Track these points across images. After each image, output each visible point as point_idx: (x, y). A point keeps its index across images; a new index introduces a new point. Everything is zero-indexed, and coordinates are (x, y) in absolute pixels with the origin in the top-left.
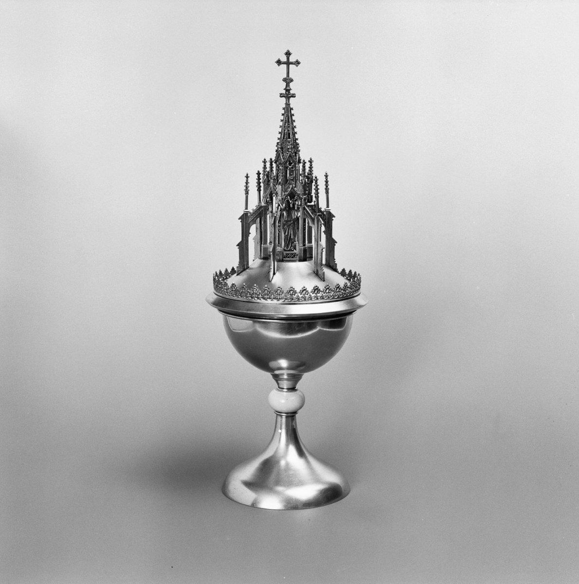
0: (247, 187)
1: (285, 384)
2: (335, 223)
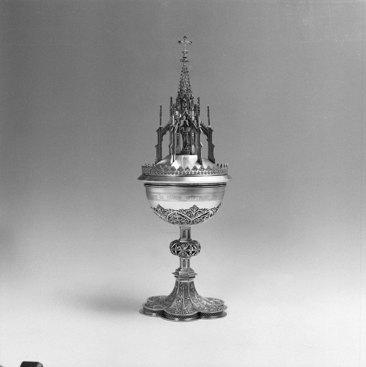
0: (161, 113)
1: (176, 254)
2: (214, 135)
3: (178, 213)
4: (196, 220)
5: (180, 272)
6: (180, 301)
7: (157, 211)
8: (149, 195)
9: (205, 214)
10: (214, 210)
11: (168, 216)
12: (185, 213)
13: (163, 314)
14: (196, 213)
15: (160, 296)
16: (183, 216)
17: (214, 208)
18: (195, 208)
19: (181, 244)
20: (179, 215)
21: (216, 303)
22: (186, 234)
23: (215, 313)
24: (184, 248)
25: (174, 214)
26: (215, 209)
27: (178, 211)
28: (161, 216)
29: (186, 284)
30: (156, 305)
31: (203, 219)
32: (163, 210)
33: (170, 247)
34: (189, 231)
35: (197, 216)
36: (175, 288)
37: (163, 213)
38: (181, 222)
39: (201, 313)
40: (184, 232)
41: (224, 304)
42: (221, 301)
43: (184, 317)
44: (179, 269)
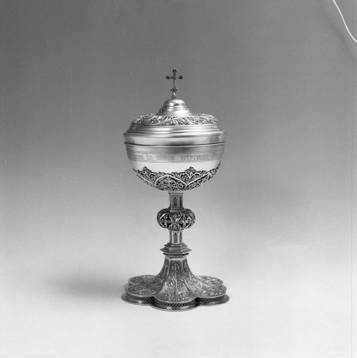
1: (166, 227)
3: (169, 177)
4: (192, 185)
5: (170, 249)
6: (172, 284)
7: (142, 174)
8: (131, 155)
9: (203, 178)
10: (213, 172)
11: (157, 181)
12: (179, 176)
13: (152, 302)
14: (192, 177)
16: (176, 181)
17: (214, 169)
18: (192, 170)
19: (172, 214)
20: (171, 179)
23: (217, 298)
24: (176, 220)
25: (165, 178)
26: (214, 170)
28: (147, 181)
29: (178, 263)
30: (142, 289)
31: (199, 183)
32: (150, 174)
33: (158, 218)
34: (181, 198)
36: (164, 268)
37: (150, 177)
38: (172, 188)
39: (200, 298)
40: (174, 199)
41: (223, 284)
42: (218, 280)
43: (181, 305)
44: (169, 245)
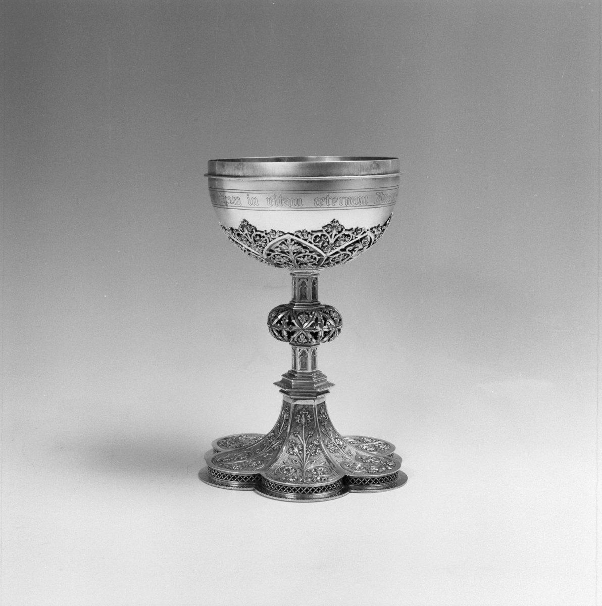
1: (286, 338)
3: (292, 240)
6: (296, 450)
7: (239, 235)
8: (217, 197)
9: (357, 242)
11: (267, 248)
13: (258, 484)
14: (337, 240)
15: (241, 436)
16: (305, 248)
17: (378, 226)
18: (335, 226)
19: (298, 314)
20: (295, 243)
21: (376, 450)
22: (307, 293)
25: (283, 243)
26: (379, 229)
27: (293, 235)
28: (249, 248)
30: (238, 459)
31: (350, 253)
32: (255, 233)
33: (270, 322)
34: (314, 282)
35: (340, 246)
36: (281, 418)
37: (255, 241)
38: (298, 262)
41: (395, 452)
42: (386, 444)
44: (291, 374)
